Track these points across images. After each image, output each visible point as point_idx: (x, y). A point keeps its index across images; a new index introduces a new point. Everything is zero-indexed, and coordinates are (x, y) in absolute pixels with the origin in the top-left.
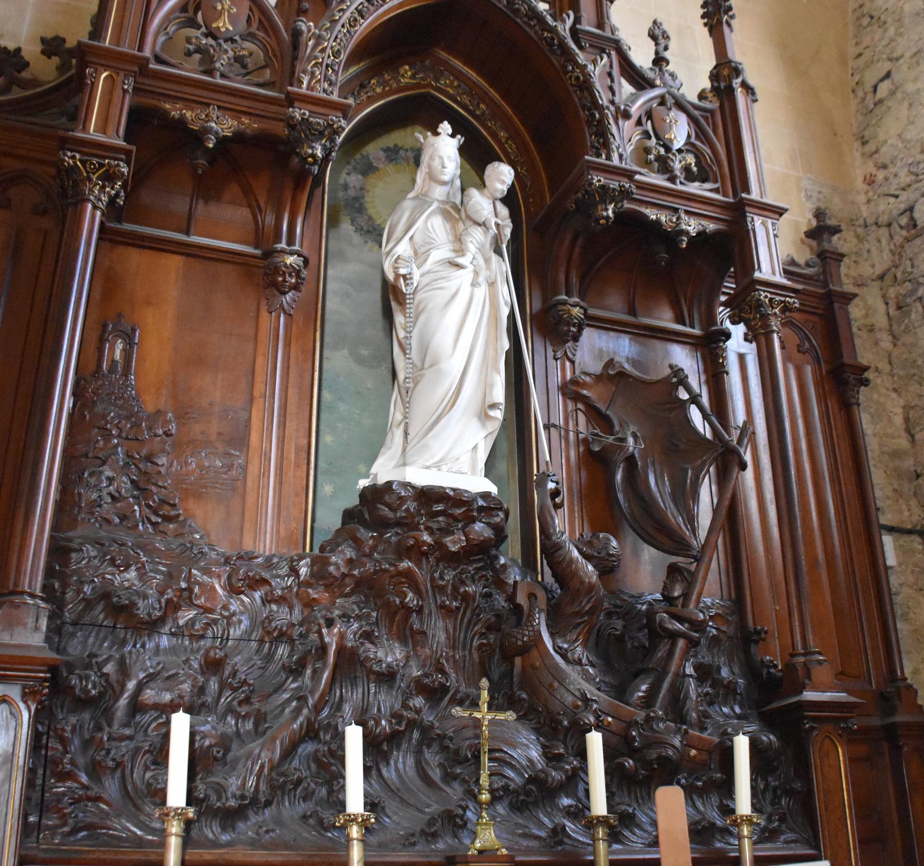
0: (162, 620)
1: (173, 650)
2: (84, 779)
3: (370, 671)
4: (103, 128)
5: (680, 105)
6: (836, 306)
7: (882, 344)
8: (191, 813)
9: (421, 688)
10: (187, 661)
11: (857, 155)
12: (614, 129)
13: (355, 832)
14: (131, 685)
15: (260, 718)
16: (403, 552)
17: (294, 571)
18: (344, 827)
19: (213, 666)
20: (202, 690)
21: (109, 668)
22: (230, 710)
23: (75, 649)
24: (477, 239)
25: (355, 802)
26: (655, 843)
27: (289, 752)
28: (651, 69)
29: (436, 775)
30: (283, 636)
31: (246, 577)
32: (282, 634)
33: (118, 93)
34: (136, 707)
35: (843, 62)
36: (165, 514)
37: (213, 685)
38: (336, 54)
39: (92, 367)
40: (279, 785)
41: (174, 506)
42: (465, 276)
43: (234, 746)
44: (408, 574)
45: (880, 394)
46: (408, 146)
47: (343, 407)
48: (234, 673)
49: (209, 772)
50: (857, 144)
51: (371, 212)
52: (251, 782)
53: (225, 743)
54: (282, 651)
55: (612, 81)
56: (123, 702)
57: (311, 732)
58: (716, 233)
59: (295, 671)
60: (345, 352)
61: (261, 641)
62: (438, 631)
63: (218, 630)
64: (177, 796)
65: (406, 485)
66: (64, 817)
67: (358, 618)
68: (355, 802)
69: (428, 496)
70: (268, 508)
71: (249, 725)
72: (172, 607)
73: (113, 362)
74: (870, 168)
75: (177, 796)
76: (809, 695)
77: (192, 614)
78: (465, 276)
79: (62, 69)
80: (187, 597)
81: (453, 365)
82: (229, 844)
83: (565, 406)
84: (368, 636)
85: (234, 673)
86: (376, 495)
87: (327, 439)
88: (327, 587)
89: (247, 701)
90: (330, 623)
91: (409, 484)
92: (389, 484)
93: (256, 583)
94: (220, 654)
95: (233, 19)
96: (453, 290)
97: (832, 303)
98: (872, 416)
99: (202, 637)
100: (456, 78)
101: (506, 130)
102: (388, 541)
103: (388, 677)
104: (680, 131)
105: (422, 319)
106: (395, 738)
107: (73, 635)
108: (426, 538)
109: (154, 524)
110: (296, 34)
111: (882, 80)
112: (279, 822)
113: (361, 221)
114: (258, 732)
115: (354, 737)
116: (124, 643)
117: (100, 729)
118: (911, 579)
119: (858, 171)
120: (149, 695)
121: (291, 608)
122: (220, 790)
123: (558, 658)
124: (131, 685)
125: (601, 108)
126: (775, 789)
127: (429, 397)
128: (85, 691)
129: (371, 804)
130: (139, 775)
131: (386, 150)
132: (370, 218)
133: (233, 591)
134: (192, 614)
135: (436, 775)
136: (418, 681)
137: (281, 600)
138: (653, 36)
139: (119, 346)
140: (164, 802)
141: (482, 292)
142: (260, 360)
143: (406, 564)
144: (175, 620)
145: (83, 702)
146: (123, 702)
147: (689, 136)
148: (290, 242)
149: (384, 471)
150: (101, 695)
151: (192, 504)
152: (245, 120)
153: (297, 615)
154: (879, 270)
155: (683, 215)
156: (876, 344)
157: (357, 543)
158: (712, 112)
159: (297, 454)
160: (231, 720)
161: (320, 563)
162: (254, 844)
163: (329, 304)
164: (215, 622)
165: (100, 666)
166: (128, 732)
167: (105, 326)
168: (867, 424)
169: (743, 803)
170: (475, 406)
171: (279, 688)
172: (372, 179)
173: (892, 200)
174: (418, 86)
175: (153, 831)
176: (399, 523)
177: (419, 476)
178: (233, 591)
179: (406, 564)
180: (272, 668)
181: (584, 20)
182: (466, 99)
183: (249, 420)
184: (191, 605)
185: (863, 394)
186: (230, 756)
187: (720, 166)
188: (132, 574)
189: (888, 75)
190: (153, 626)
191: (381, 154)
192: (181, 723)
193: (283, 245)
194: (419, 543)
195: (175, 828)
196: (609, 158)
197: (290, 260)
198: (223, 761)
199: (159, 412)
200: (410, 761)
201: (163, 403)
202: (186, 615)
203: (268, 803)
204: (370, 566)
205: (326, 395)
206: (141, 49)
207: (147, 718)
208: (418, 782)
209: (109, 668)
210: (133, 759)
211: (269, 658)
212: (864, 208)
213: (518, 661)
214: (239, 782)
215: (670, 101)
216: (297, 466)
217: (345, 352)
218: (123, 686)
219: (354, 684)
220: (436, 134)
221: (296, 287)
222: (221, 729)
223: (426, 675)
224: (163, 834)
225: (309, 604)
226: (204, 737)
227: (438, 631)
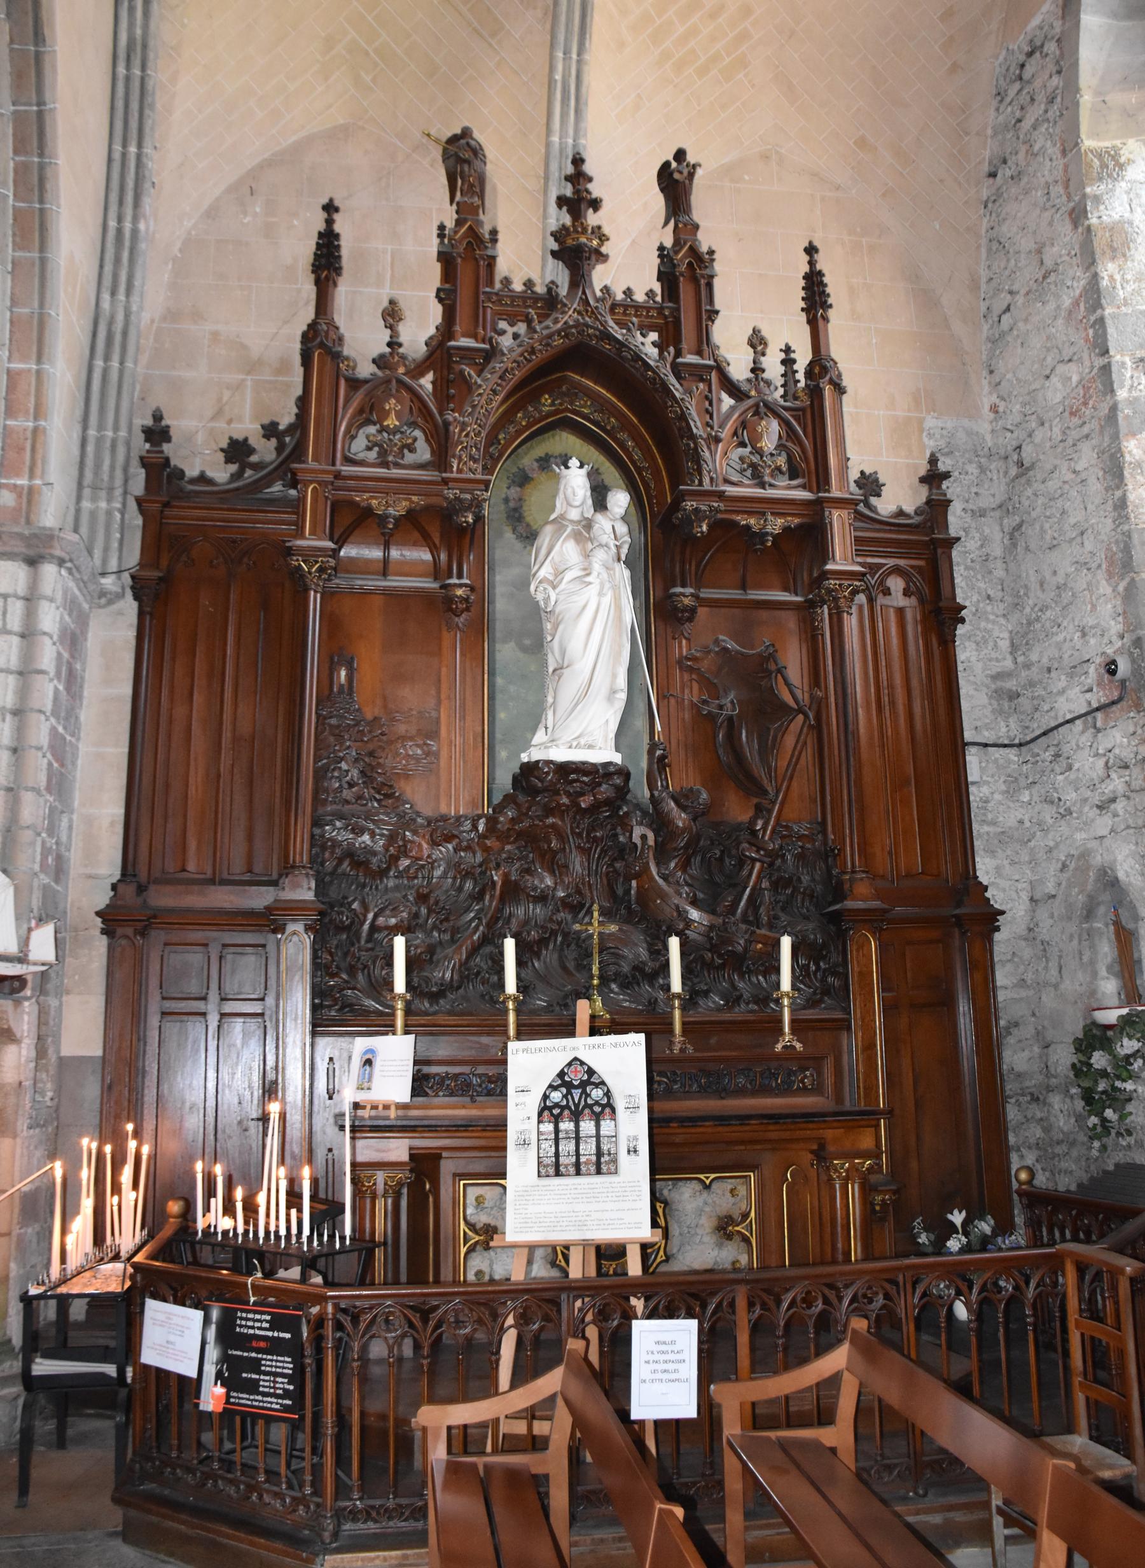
0: (388, 869)
1: (397, 888)
2: (344, 976)
3: (528, 895)
4: (316, 459)
5: (772, 410)
6: (939, 551)
7: (995, 573)
8: (408, 996)
9: (565, 904)
10: (405, 896)
11: (985, 382)
12: (706, 454)
13: (511, 1005)
14: (370, 916)
15: (455, 931)
16: (549, 811)
17: (475, 827)
18: (504, 1002)
19: (422, 898)
20: (416, 915)
21: (355, 906)
22: (434, 927)
23: (333, 893)
24: (600, 557)
25: (511, 986)
26: (594, 1032)
27: (471, 954)
28: (749, 380)
29: (571, 965)
30: (468, 874)
31: (442, 830)
32: (467, 873)
33: (321, 500)
34: (374, 928)
35: (975, 286)
36: (387, 793)
37: (424, 911)
38: (478, 434)
39: (326, 693)
40: (466, 974)
41: (391, 787)
42: (593, 590)
43: (438, 950)
44: (553, 826)
45: (987, 620)
46: (556, 453)
47: (512, 688)
48: (437, 903)
49: (422, 969)
50: (985, 373)
51: (529, 519)
52: (448, 975)
53: (431, 950)
54: (469, 885)
55: (711, 404)
56: (366, 927)
57: (485, 940)
58: (800, 527)
59: (479, 897)
60: (512, 644)
61: (455, 878)
62: (577, 864)
63: (425, 872)
64: (400, 986)
65: (548, 762)
66: (336, 1000)
67: (519, 859)
68: (511, 986)
69: (565, 769)
70: (450, 787)
71: (447, 937)
72: (394, 859)
73: (341, 686)
74: (994, 399)
75: (400, 986)
76: (849, 904)
77: (407, 862)
78: (593, 590)
79: (280, 449)
80: (404, 852)
81: (582, 666)
82: (435, 1013)
83: (682, 677)
84: (528, 871)
85: (437, 903)
86: (530, 769)
87: (501, 715)
88: (498, 838)
89: (447, 920)
90: (498, 866)
91: (551, 762)
92: (538, 762)
93: (448, 838)
94: (426, 891)
95: (399, 416)
96: (582, 604)
97: (935, 549)
98: (978, 644)
99: (416, 877)
100: (590, 398)
101: (634, 439)
102: (538, 803)
103: (542, 898)
104: (770, 433)
105: (561, 628)
106: (543, 942)
107: (331, 882)
108: (565, 800)
109: (379, 801)
110: (446, 424)
111: (1004, 312)
112: (465, 998)
113: (521, 529)
114: (453, 941)
115: (510, 944)
116: (364, 886)
117: (353, 945)
118: (1003, 788)
119: (985, 400)
120: (381, 921)
121: (474, 853)
122: (427, 980)
123: (660, 881)
124: (370, 916)
125: (693, 437)
126: (825, 970)
127: (569, 688)
128: (341, 921)
129: (522, 986)
130: (379, 972)
131: (538, 460)
132: (528, 525)
133: (434, 844)
134: (407, 862)
135: (571, 965)
136: (562, 899)
137: (468, 848)
138: (752, 345)
139: (343, 673)
140: (392, 990)
141: (607, 599)
142: (444, 670)
143: (551, 820)
144: (397, 867)
145: (341, 928)
146: (366, 927)
147: (780, 437)
148: (460, 576)
149: (534, 754)
150: (352, 923)
151: (402, 783)
152: (415, 498)
153: (479, 858)
154: (998, 501)
155: (770, 517)
156: (990, 572)
157: (518, 806)
158: (803, 410)
159: (475, 739)
160: (436, 934)
161: (492, 821)
162: (450, 1013)
163: (300, 1071)
164: (423, 866)
165: (350, 904)
166: (369, 945)
167: (332, 659)
168: (966, 653)
169: (786, 984)
170: (604, 691)
171: (468, 910)
172: (529, 488)
173: (1008, 434)
174: (557, 412)
175: (388, 1007)
176: (545, 790)
177: (560, 754)
178: (434, 844)
179: (551, 820)
180: (462, 896)
181: (684, 351)
182: (597, 416)
183: (438, 718)
184: (407, 856)
185: (961, 630)
186: (435, 958)
187: (807, 463)
188: (366, 838)
189: (1008, 309)
190: (383, 873)
191: (536, 465)
192: (399, 943)
193: (454, 581)
194: (559, 805)
195: (400, 1005)
196: (701, 484)
197: (460, 592)
198: (431, 961)
199: (375, 719)
200: (556, 956)
201: (377, 712)
202: (404, 863)
203: (459, 988)
204: (526, 824)
205: (499, 681)
206: (334, 464)
207: (383, 935)
208: (560, 970)
209: (355, 906)
210: (374, 963)
211: (460, 889)
212: (988, 437)
213: (634, 883)
214: (446, 973)
215: (762, 409)
216: (475, 748)
217: (512, 644)
218: (365, 917)
219: (518, 903)
220: (567, 467)
221: (468, 609)
222: (428, 941)
223: (568, 896)
224: (393, 1008)
225: (486, 850)
226: (416, 947)
227: (577, 864)
